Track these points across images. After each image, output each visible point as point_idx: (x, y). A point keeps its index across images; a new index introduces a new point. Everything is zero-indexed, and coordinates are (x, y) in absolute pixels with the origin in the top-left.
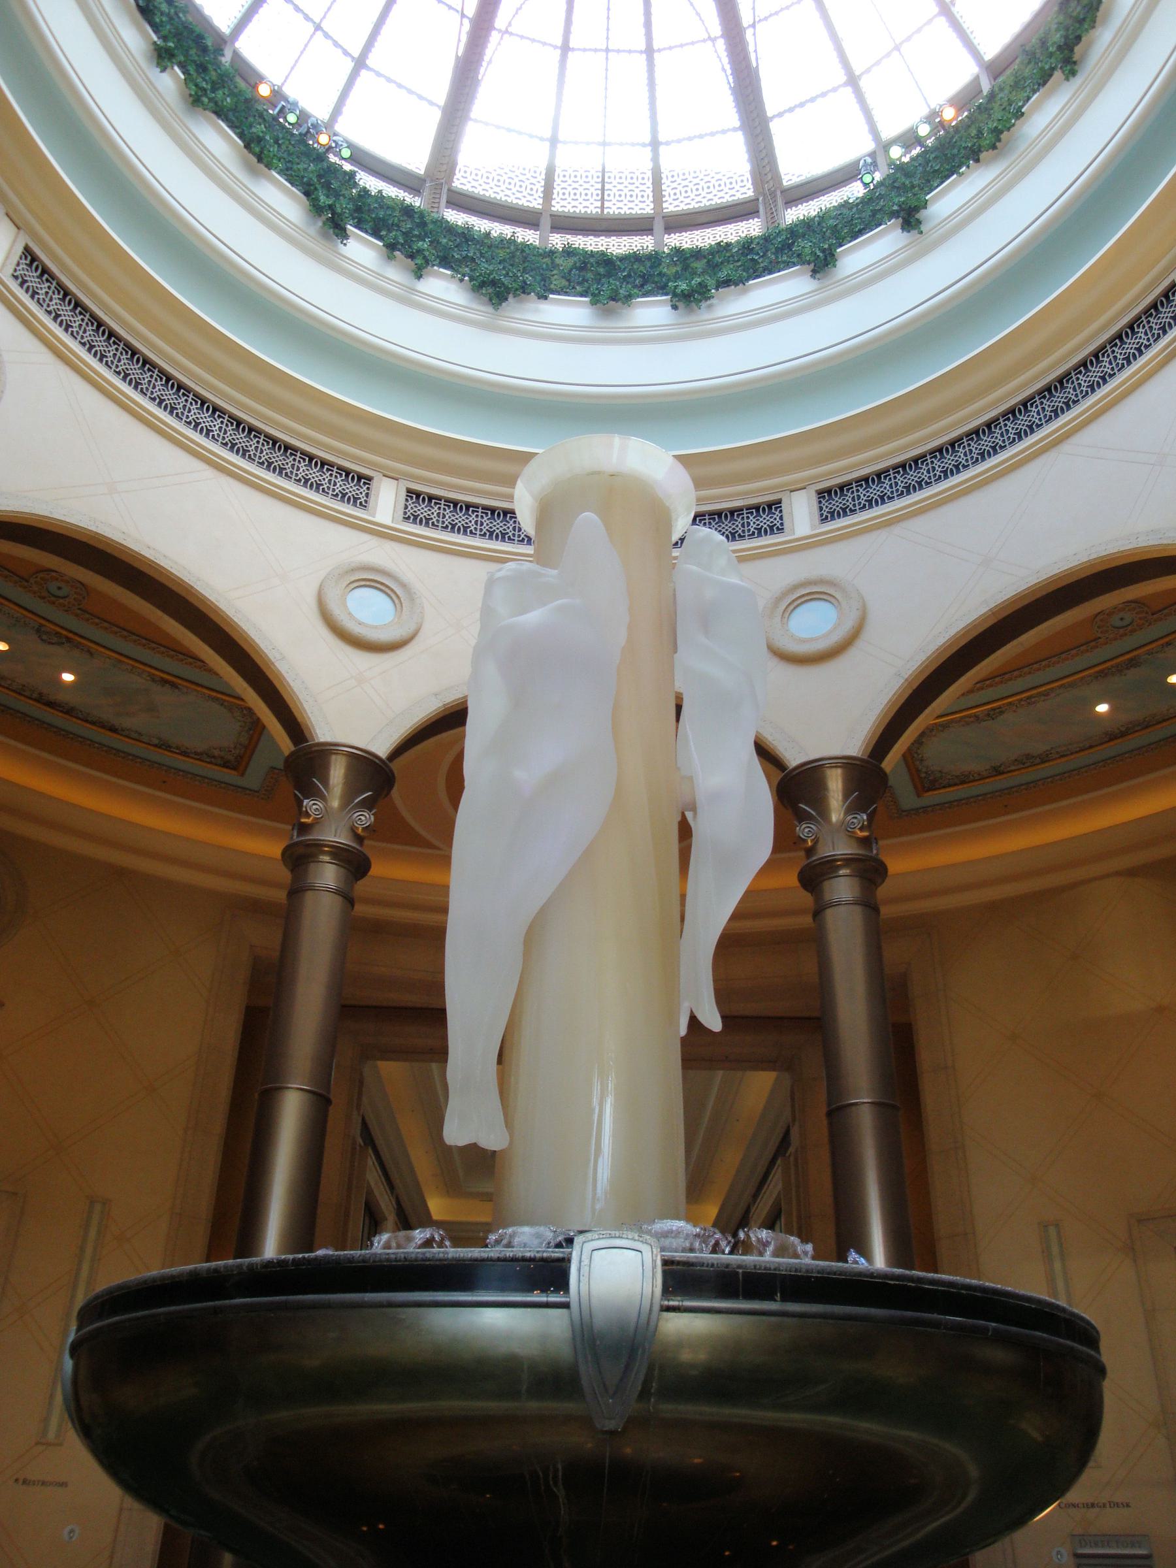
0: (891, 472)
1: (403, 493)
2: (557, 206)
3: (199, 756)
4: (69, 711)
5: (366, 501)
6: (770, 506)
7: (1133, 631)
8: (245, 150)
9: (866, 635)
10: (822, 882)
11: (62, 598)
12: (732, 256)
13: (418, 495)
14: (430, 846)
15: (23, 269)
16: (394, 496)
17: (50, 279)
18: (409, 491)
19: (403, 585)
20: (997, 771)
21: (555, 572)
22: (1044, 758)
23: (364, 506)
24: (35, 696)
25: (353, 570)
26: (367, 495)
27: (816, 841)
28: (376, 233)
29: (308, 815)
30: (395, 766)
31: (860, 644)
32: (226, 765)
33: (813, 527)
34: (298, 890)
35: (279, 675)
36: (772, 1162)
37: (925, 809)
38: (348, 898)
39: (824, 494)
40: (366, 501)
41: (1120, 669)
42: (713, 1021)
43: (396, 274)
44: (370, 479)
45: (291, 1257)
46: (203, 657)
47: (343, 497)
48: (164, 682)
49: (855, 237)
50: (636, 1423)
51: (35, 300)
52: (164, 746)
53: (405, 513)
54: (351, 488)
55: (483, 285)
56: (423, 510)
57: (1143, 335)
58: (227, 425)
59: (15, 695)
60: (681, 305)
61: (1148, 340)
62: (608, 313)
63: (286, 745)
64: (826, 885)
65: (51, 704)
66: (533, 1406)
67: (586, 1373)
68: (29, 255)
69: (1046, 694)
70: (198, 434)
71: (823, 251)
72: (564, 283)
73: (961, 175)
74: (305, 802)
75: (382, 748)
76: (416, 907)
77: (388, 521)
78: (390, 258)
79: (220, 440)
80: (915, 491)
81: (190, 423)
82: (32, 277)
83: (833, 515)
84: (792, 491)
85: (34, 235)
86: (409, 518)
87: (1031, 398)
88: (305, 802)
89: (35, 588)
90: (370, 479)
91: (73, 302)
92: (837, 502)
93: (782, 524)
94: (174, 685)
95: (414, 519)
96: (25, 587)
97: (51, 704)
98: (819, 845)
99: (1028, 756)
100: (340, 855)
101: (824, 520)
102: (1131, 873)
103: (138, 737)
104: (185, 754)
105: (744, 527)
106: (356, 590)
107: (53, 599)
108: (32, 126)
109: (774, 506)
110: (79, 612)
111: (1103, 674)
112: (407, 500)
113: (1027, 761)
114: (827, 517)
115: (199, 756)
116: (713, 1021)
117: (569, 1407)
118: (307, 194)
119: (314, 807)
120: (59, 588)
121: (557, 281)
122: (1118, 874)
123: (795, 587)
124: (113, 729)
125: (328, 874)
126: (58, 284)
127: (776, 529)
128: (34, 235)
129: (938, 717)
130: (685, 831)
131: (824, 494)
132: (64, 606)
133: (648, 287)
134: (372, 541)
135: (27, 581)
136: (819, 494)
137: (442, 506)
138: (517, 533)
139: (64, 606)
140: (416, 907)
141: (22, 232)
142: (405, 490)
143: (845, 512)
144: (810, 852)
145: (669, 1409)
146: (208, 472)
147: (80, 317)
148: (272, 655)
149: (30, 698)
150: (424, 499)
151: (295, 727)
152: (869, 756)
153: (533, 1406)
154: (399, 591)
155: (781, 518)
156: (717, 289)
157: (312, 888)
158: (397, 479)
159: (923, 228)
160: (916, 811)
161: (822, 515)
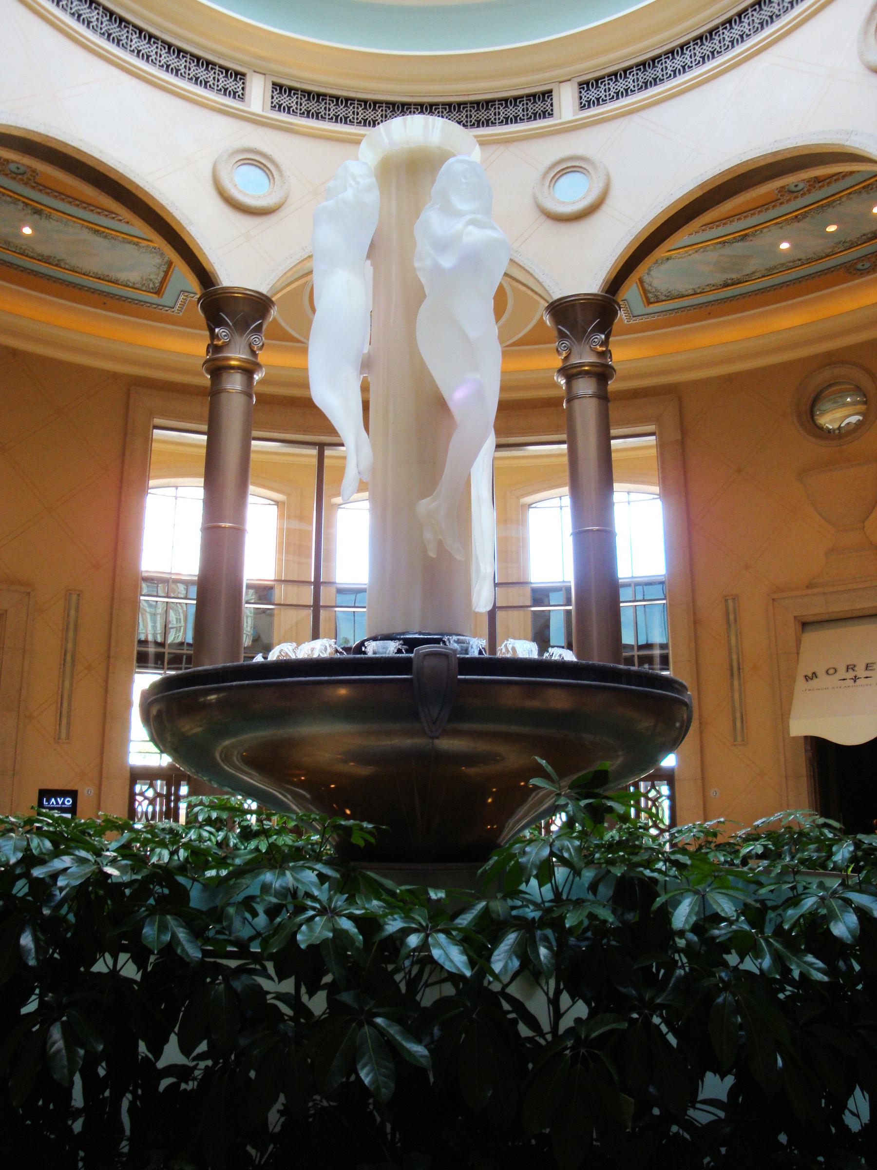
1: (270, 86)
5: (242, 94)
7: (802, 195)
11: (21, 174)
13: (281, 87)
16: (261, 102)
23: (242, 98)
24: (21, 251)
26: (243, 89)
27: (226, 345)
31: (605, 209)
39: (584, 85)
40: (242, 94)
44: (244, 75)
45: (157, 924)
47: (225, 91)
53: (272, 103)
54: (231, 84)
56: (285, 100)
59: (70, 272)
63: (193, 284)
74: (217, 330)
80: (651, 86)
81: (103, 34)
84: (561, 82)
86: (275, 107)
87: (687, 43)
88: (217, 330)
90: (244, 75)
92: (593, 94)
93: (552, 110)
95: (278, 107)
101: (582, 107)
109: (547, 94)
112: (273, 92)
114: (585, 105)
119: (224, 334)
127: (546, 114)
131: (584, 85)
134: (249, 127)
136: (580, 85)
138: (356, 117)
143: (598, 101)
148: (184, 222)
149: (15, 252)
151: (205, 277)
152: (606, 293)
155: (552, 105)
158: (264, 74)
161: (581, 103)
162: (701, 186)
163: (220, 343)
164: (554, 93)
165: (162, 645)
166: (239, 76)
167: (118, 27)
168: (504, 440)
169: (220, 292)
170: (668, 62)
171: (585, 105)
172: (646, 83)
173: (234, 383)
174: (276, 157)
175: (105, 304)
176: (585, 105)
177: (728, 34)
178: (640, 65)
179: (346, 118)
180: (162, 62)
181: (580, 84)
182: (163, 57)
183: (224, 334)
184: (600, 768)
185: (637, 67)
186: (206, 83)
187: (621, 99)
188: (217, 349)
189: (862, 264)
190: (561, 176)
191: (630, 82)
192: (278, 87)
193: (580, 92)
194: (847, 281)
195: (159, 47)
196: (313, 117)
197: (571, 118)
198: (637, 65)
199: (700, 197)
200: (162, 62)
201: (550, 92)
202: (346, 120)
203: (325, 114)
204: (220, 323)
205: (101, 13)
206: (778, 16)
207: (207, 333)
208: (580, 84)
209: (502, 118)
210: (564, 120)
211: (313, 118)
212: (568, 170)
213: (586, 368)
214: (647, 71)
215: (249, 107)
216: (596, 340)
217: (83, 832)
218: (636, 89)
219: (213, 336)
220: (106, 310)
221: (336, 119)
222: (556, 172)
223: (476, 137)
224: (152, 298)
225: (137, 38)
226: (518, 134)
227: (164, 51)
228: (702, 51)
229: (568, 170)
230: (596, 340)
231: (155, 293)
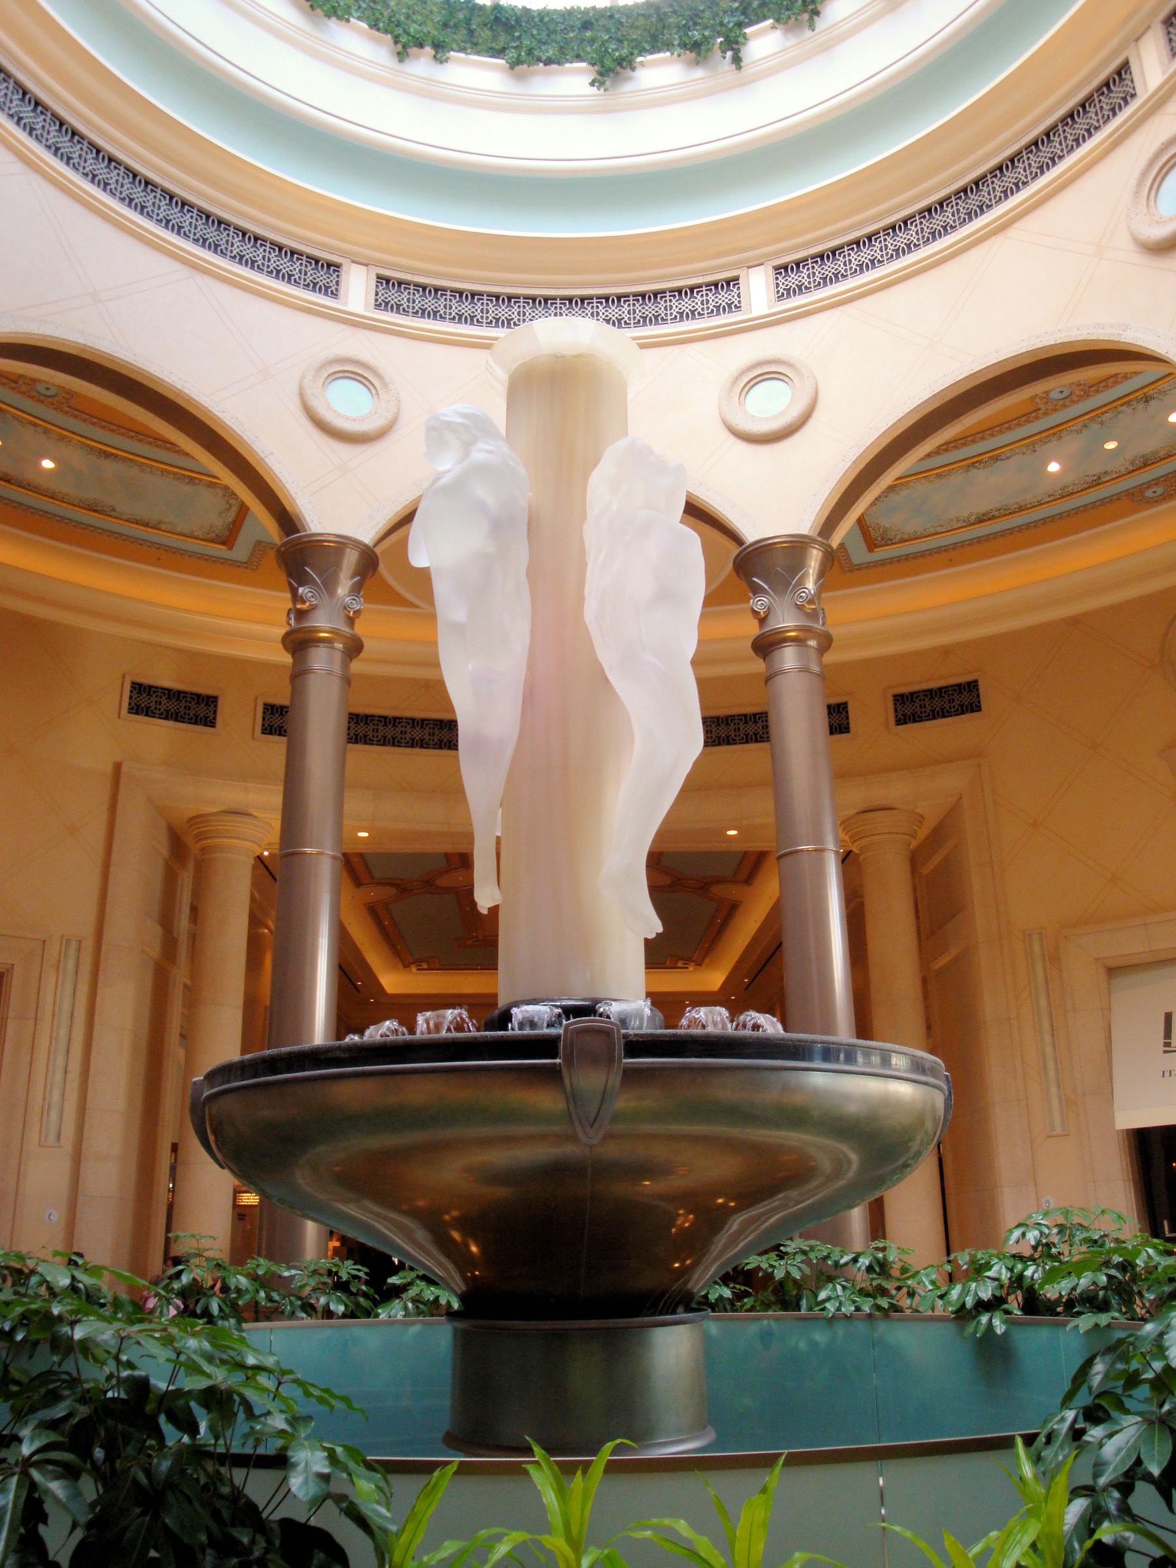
0: (846, 249)
5: (337, 290)
9: (821, 405)
10: (773, 651)
14: (404, 602)
15: (54, 137)
17: (44, 111)
18: (380, 277)
23: (335, 295)
27: (314, 608)
30: (378, 550)
31: (812, 423)
34: (299, 674)
39: (782, 269)
44: (338, 266)
51: (34, 136)
53: (376, 300)
54: (322, 276)
56: (393, 296)
57: (1057, 145)
58: (197, 219)
61: (1062, 150)
63: (271, 531)
64: (776, 654)
70: (169, 233)
74: (301, 590)
76: (53, 603)
79: (192, 236)
83: (789, 293)
84: (749, 267)
87: (983, 177)
88: (301, 590)
89: (23, 389)
90: (338, 266)
91: (70, 132)
92: (793, 279)
96: (13, 389)
98: (770, 617)
101: (780, 297)
105: (703, 304)
106: (336, 381)
107: (42, 398)
109: (732, 282)
110: (67, 409)
112: (377, 286)
120: (48, 389)
126: (53, 115)
127: (731, 307)
129: (897, 479)
131: (782, 269)
132: (53, 404)
135: (16, 382)
137: (412, 291)
139: (53, 404)
140: (53, 603)
142: (375, 277)
144: (762, 621)
147: (42, 117)
150: (393, 284)
151: (287, 520)
155: (739, 296)
158: (366, 265)
160: (868, 566)
163: (305, 606)
166: (333, 267)
167: (106, 168)
168: (881, 1234)
169: (304, 540)
170: (852, 254)
172: (933, 234)
173: (321, 660)
174: (372, 362)
177: (963, 205)
178: (1030, 146)
179: (472, 318)
180: (161, 216)
181: (776, 268)
182: (162, 209)
183: (310, 594)
185: (991, 173)
186: (290, 276)
188: (301, 615)
189: (1157, 494)
190: (756, 384)
192: (383, 280)
193: (777, 279)
194: (1128, 514)
195: (122, 174)
196: (429, 317)
197: (767, 311)
198: (1027, 147)
199: (939, 407)
200: (161, 216)
201: (736, 279)
202: (471, 320)
203: (445, 313)
204: (303, 580)
205: (85, 148)
206: (1024, 183)
207: (289, 595)
208: (776, 268)
209: (675, 313)
210: (755, 314)
211: (429, 317)
212: (771, 376)
213: (793, 634)
214: (1005, 176)
215: (346, 304)
216: (803, 595)
218: (921, 242)
219: (296, 597)
220: (159, 567)
221: (460, 318)
222: (752, 376)
223: (634, 339)
224: (219, 551)
225: (130, 183)
227: (164, 203)
228: (967, 206)
229: (771, 376)
230: (803, 595)
231: (223, 543)
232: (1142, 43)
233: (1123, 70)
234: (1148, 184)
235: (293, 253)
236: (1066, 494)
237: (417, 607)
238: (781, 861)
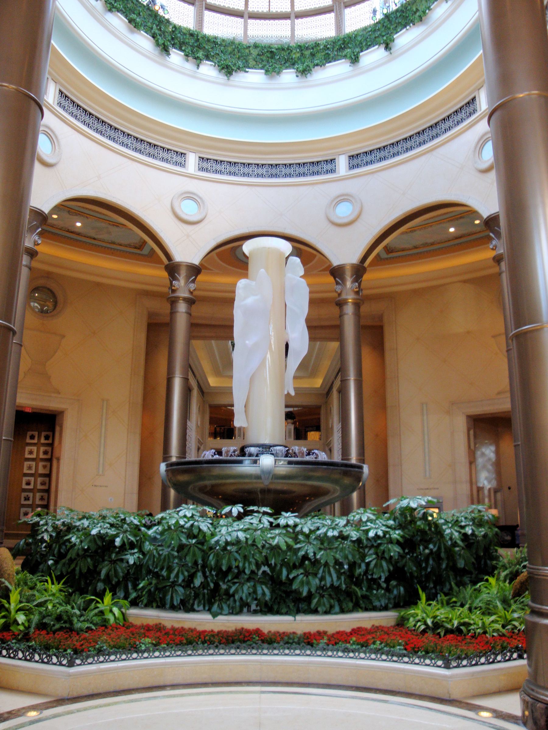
1: (198, 158)
2: (250, 9)
3: (126, 246)
4: (78, 234)
6: (331, 160)
8: (129, 24)
12: (320, 49)
13: (203, 159)
14: (209, 269)
19: (200, 198)
20: (416, 248)
21: (254, 282)
22: (432, 244)
25: (182, 194)
28: (180, 49)
29: (174, 286)
31: (357, 223)
32: (135, 248)
33: (346, 172)
35: (161, 238)
36: (338, 374)
37: (390, 258)
38: (189, 314)
39: (351, 157)
41: (457, 219)
42: (293, 393)
43: (189, 66)
44: (185, 154)
46: (131, 228)
48: (113, 225)
49: (367, 49)
50: (271, 483)
52: (114, 243)
54: (179, 159)
55: (223, 68)
56: (205, 165)
60: (299, 75)
62: (272, 77)
65: (72, 232)
66: (255, 481)
67: (263, 476)
68: (61, 92)
69: (431, 226)
71: (354, 55)
72: (254, 63)
73: (407, 30)
74: (174, 282)
75: (196, 261)
77: (193, 173)
78: (187, 60)
82: (66, 103)
85: (62, 85)
88: (174, 282)
92: (355, 162)
94: (117, 226)
95: (202, 169)
97: (72, 232)
99: (426, 243)
100: (185, 300)
102: (465, 282)
103: (103, 241)
104: (121, 245)
108: (61, 50)
109: (332, 161)
111: (452, 220)
113: (426, 245)
115: (126, 246)
116: (293, 393)
117: (259, 481)
118: (153, 37)
121: (252, 63)
122: (460, 282)
123: (338, 197)
124: (94, 239)
125: (182, 307)
127: (333, 171)
128: (62, 85)
130: (287, 346)
131: (351, 157)
133: (287, 65)
141: (57, 84)
143: (358, 166)
145: (276, 481)
146: (129, 162)
153: (255, 481)
154: (199, 200)
156: (314, 68)
157: (178, 312)
159: (392, 51)
160: (387, 259)
162: (404, 214)
164: (336, 160)
165: (220, 600)
171: (352, 167)
175: (509, 488)
176: (352, 167)
184: (527, 666)
187: (395, 157)
191: (425, 137)
208: (350, 156)
217: (155, 645)
226: (17, 290)
232: (480, 90)
233: (474, 99)
234: (478, 149)
235: (168, 150)
236: (457, 238)
237: (212, 270)
238: (262, 522)
